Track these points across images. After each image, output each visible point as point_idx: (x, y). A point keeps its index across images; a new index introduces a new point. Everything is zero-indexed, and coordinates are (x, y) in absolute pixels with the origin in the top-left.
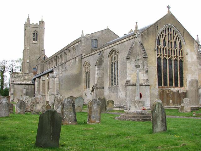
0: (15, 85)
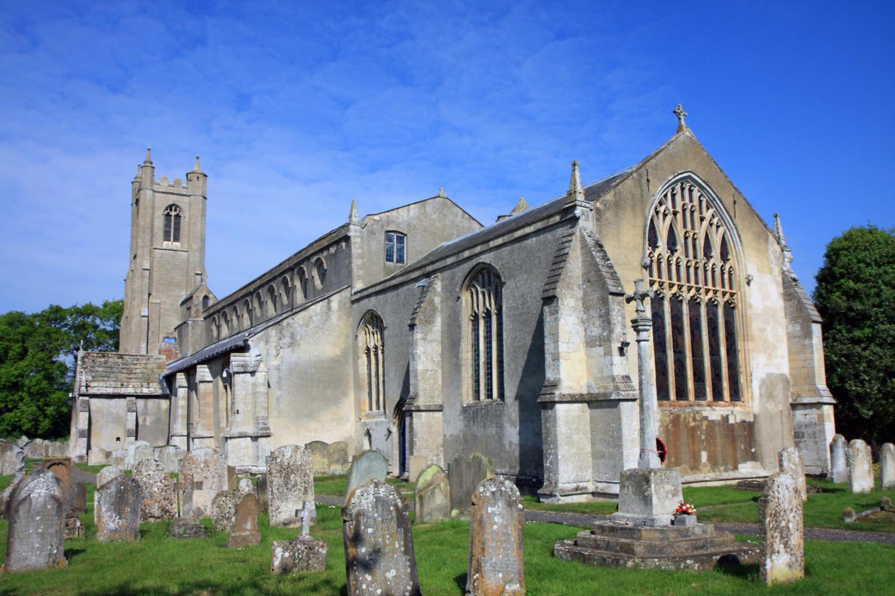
0: (94, 402)
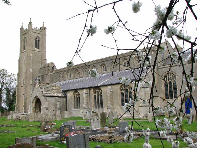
0: (47, 98)
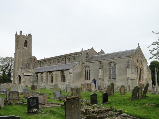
0: (25, 76)
